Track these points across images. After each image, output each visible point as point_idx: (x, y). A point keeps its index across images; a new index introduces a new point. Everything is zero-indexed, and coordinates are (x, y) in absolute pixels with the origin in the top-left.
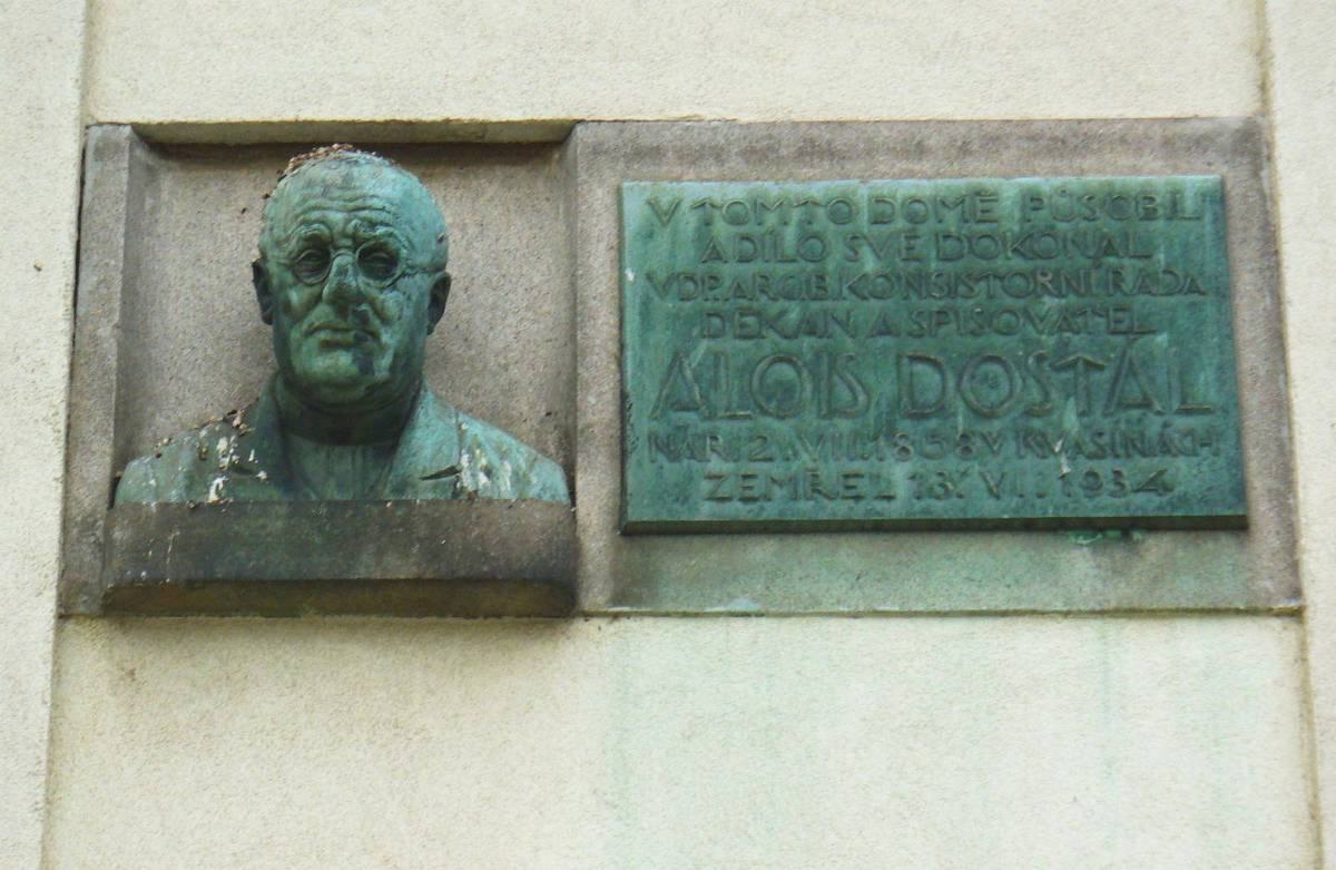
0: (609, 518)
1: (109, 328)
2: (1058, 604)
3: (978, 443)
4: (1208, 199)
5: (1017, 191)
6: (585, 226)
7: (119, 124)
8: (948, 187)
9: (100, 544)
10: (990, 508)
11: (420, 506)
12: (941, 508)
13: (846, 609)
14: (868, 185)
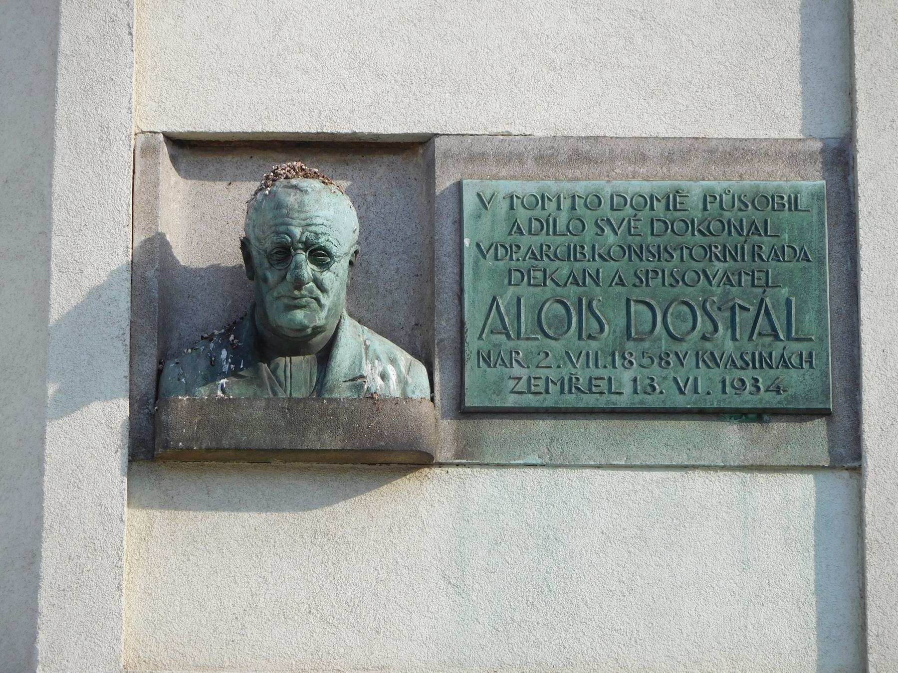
0: (454, 402)
1: (153, 271)
2: (718, 461)
3: (672, 359)
4: (815, 197)
5: (701, 190)
6: (440, 207)
7: (155, 133)
8: (659, 187)
9: (151, 414)
10: (680, 402)
11: (344, 402)
12: (652, 401)
13: (593, 463)
14: (611, 184)
